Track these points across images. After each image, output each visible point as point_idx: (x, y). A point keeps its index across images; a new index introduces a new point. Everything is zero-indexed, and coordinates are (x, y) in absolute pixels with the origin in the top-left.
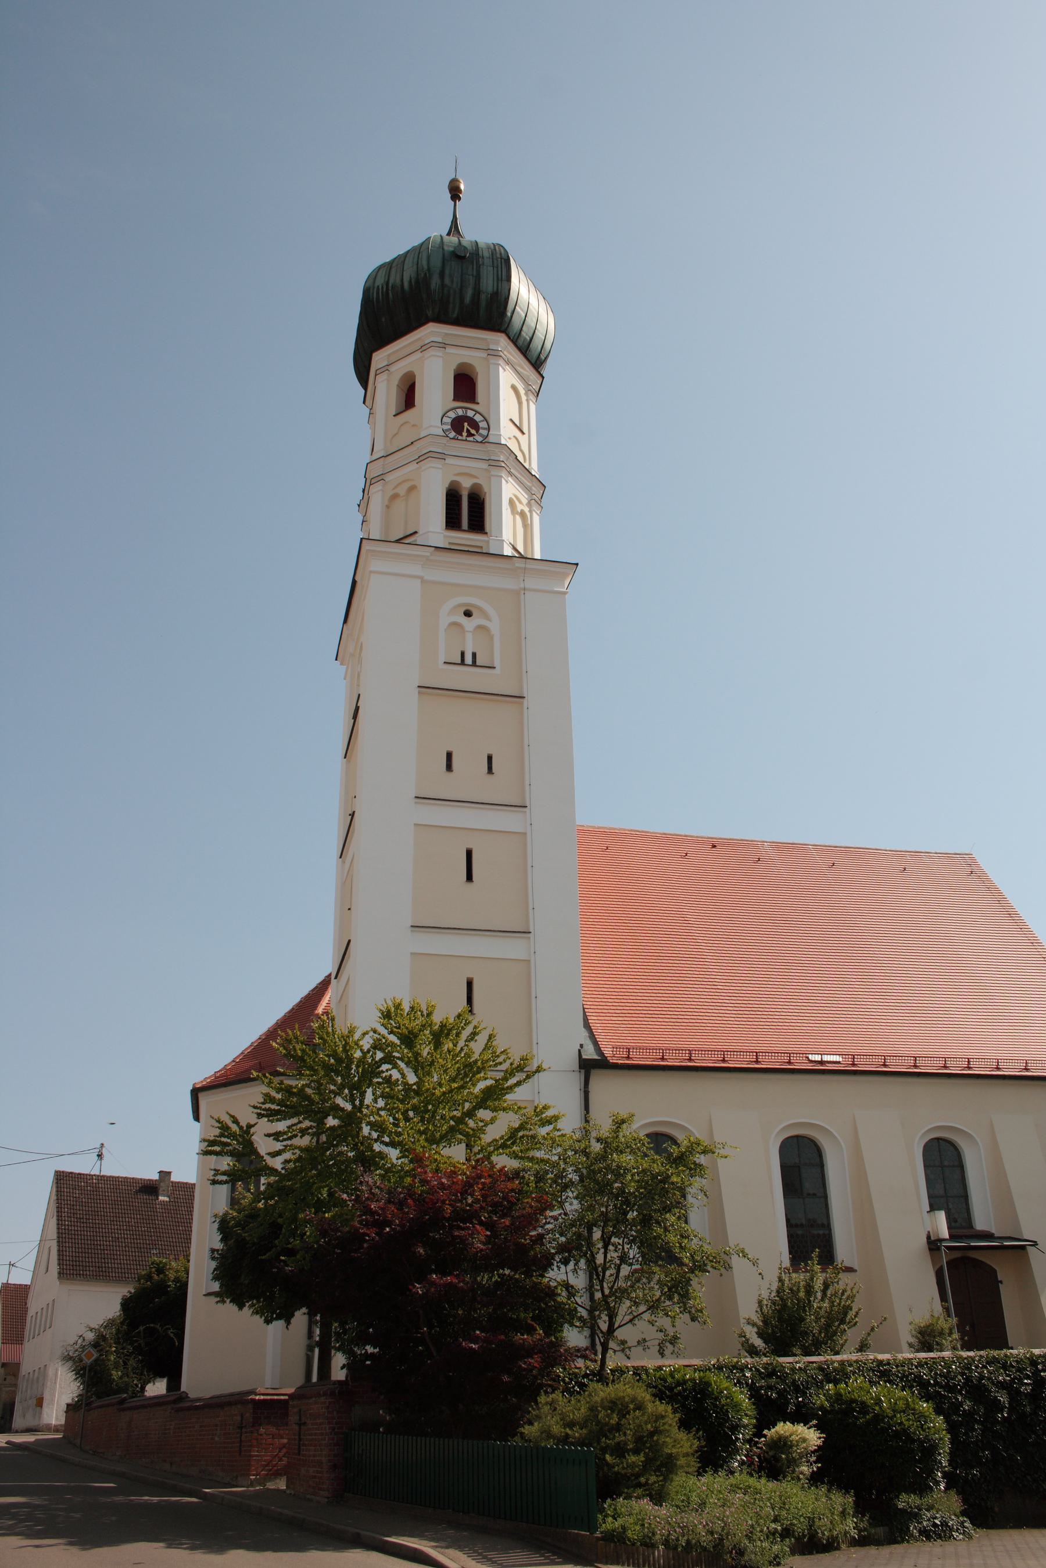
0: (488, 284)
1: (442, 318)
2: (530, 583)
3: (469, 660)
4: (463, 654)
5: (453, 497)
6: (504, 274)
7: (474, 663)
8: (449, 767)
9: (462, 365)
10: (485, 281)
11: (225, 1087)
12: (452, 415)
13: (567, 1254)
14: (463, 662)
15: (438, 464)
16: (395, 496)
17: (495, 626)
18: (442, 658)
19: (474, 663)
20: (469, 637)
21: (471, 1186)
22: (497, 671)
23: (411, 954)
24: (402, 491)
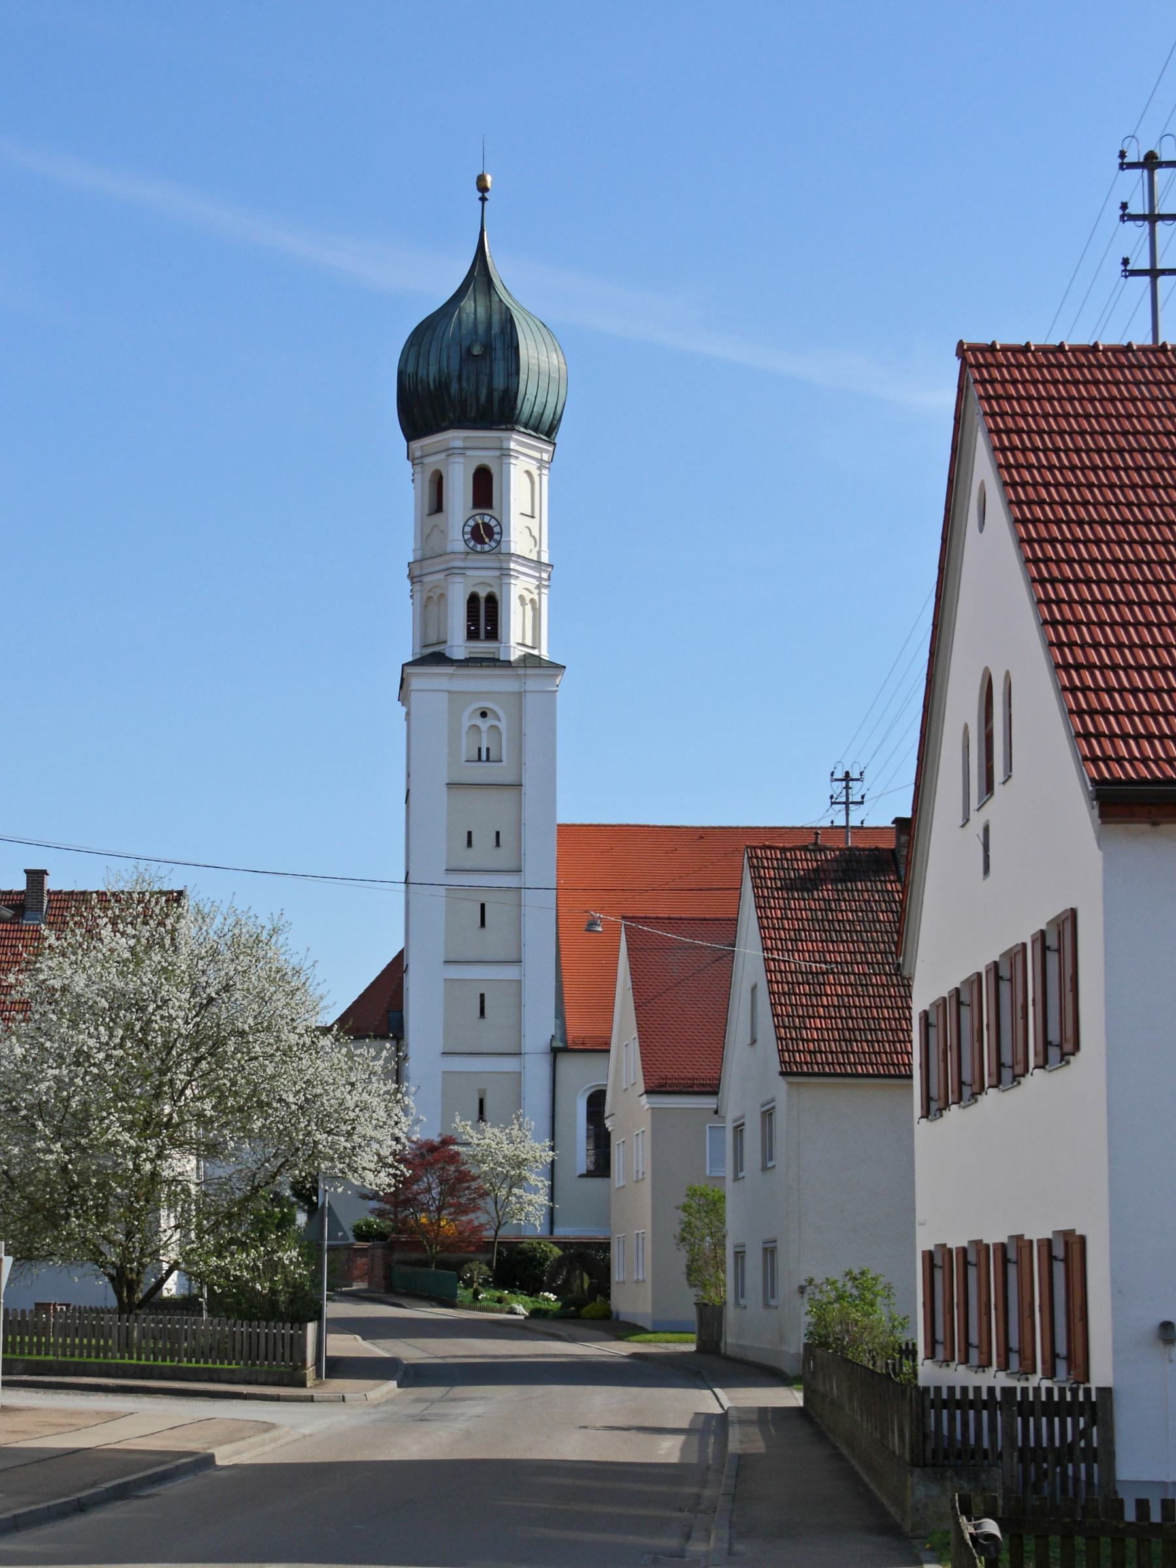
0: (499, 382)
1: (461, 423)
2: (531, 685)
3: (484, 757)
4: (480, 749)
5: (473, 599)
6: (514, 367)
7: (488, 760)
8: (469, 844)
10: (180, 1481)
11: (938, 582)
14: (480, 759)
16: (430, 598)
17: (503, 726)
18: (464, 758)
19: (488, 760)
20: (484, 736)
21: (213, 1122)
22: (504, 764)
23: (445, 980)
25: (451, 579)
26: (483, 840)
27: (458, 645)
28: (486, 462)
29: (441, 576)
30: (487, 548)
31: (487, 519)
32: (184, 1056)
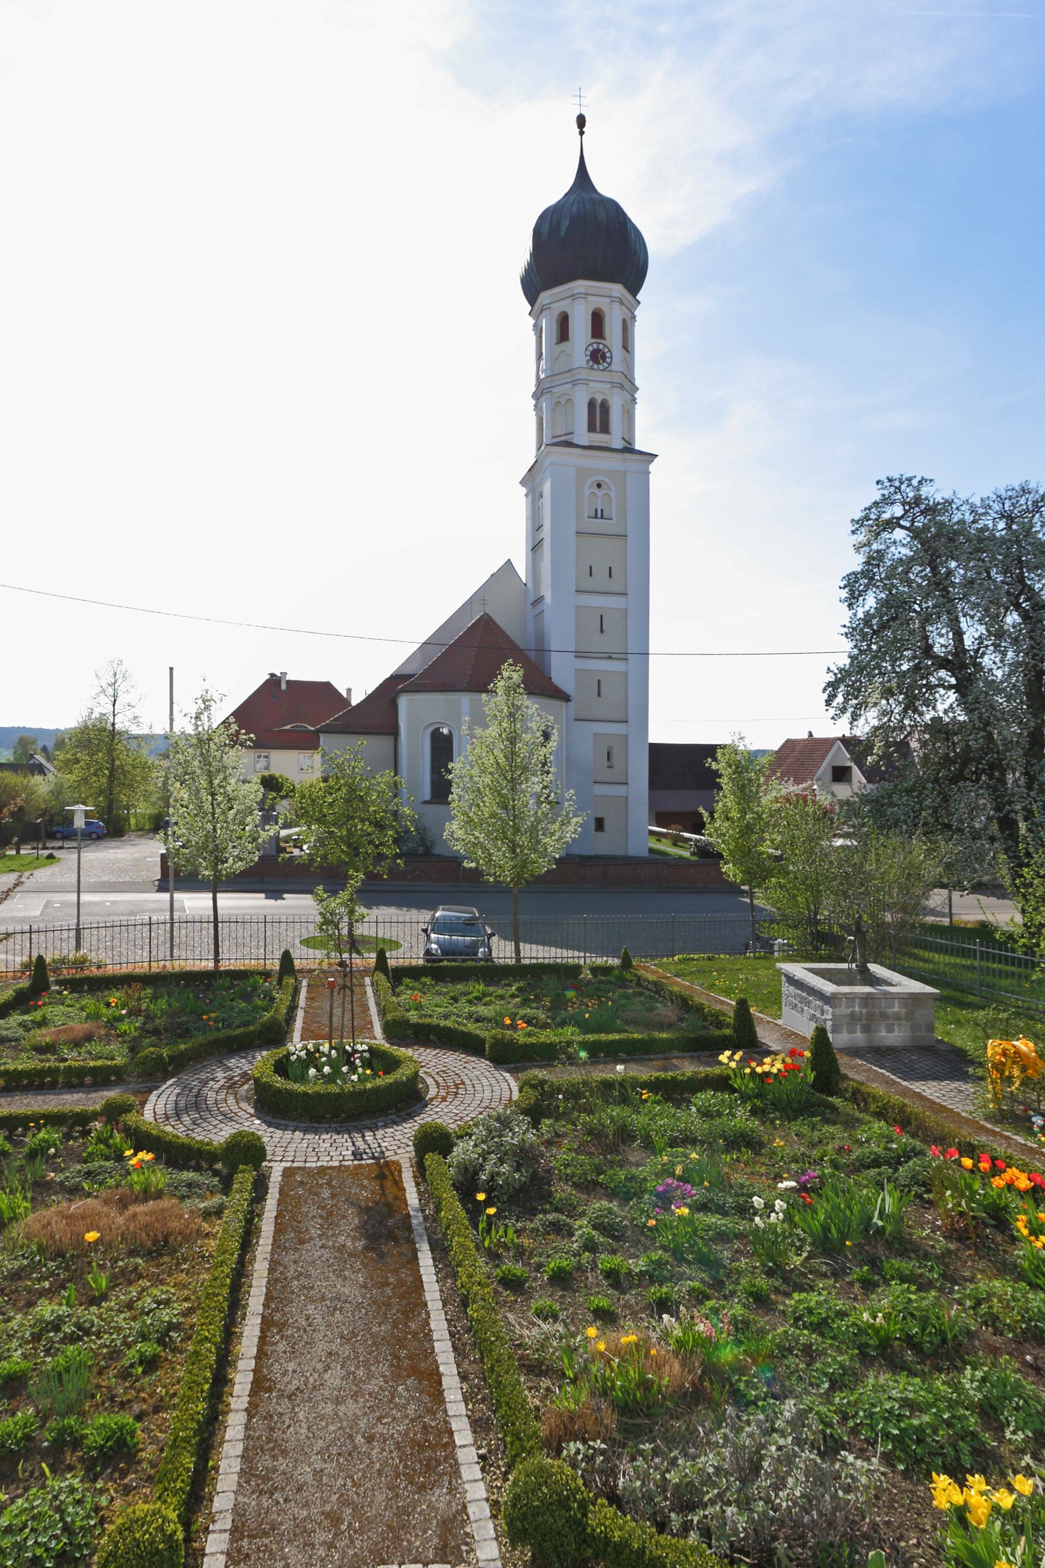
5: (591, 404)
7: (602, 517)
9: (598, 309)
12: (590, 348)
13: (977, 825)
14: (596, 517)
15: (584, 387)
17: (613, 494)
18: (586, 515)
24: (563, 400)
25: (577, 388)
26: (601, 572)
27: (583, 436)
28: (601, 306)
29: (569, 386)
30: (601, 367)
31: (601, 347)
32: (865, 1182)
